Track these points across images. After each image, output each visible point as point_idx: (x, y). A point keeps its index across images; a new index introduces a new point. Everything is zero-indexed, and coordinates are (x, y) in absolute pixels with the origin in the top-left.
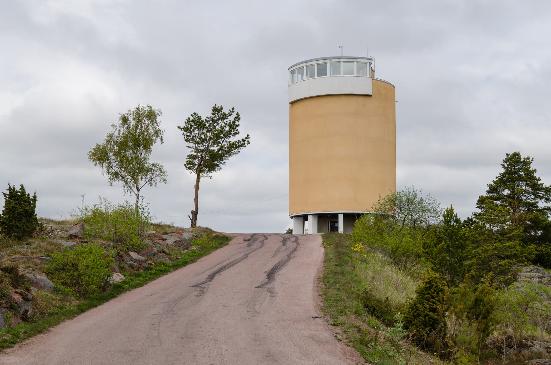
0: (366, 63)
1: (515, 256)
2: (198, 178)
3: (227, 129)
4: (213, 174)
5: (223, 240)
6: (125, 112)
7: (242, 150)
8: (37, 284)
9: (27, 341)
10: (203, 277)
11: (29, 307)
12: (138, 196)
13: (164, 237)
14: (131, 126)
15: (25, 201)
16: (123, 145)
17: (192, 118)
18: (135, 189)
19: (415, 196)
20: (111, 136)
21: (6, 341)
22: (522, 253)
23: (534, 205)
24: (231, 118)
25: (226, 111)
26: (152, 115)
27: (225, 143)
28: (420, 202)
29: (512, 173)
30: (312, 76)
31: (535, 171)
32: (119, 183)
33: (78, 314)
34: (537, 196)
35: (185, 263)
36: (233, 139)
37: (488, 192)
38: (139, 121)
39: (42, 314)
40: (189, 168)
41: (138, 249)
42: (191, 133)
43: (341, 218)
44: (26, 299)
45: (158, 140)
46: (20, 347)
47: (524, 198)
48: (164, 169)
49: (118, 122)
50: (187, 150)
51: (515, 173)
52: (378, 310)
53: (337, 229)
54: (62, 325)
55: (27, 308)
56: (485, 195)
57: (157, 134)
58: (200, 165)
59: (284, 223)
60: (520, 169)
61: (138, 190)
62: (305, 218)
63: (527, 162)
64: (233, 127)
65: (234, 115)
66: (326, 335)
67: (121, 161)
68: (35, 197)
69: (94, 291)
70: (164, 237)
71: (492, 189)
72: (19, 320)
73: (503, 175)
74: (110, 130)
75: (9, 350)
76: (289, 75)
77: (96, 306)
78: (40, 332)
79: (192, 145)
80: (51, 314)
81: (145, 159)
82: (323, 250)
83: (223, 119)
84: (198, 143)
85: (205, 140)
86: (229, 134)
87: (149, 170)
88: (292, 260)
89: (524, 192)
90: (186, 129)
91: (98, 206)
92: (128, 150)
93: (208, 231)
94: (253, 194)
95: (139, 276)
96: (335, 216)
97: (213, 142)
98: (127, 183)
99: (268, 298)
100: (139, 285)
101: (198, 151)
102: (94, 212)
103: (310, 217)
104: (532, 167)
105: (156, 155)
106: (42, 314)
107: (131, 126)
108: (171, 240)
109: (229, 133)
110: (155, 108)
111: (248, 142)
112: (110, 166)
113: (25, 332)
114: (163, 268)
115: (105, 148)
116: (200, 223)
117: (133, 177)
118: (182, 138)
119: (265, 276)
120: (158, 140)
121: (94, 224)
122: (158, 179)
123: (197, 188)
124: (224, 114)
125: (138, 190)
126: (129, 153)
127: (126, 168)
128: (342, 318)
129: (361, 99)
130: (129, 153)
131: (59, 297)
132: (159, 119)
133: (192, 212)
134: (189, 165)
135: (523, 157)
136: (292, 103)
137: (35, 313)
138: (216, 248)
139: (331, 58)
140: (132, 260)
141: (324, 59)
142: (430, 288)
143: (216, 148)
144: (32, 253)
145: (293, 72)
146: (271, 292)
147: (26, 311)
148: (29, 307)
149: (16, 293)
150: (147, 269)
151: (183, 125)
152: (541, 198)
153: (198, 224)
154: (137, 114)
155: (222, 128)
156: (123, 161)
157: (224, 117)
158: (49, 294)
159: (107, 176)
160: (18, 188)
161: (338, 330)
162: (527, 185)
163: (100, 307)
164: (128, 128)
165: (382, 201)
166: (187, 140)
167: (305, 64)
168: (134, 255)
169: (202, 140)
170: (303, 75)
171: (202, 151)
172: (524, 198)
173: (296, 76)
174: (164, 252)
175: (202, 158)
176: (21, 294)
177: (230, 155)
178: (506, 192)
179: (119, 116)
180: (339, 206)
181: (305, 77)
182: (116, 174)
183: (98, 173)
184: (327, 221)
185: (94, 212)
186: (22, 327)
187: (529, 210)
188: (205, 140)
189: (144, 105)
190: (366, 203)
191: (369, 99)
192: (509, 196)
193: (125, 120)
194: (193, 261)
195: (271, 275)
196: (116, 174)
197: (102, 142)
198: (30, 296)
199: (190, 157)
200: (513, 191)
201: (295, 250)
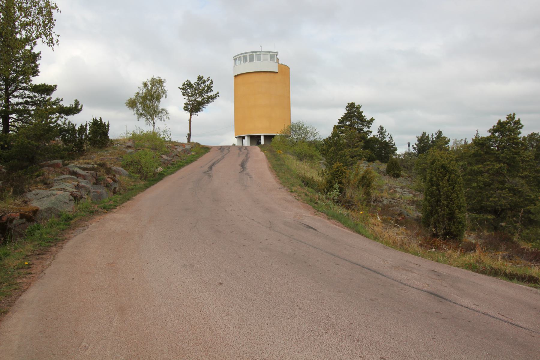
0: (274, 55)
1: (359, 155)
2: (191, 116)
3: (206, 88)
4: (199, 113)
5: (207, 149)
6: (145, 80)
7: (215, 100)
8: (119, 173)
9: (123, 205)
10: (206, 168)
11: (116, 185)
12: (154, 126)
13: (176, 147)
14: (149, 88)
15: (103, 127)
16: (144, 98)
17: (186, 83)
18: (152, 123)
19: (303, 125)
20: (138, 93)
21: (111, 205)
22: (363, 153)
23: (362, 130)
24: (208, 83)
25: (205, 78)
26: (160, 82)
27: (205, 96)
28: (306, 129)
29: (350, 113)
30: (246, 61)
31: (362, 112)
32: (143, 120)
33: (146, 189)
34: (363, 125)
35: (191, 162)
36: (209, 94)
37: (338, 123)
38: (153, 85)
39: (125, 189)
40: (186, 110)
41: (166, 153)
42: (186, 91)
43: (262, 138)
44: (115, 181)
45: (164, 95)
46: (120, 208)
47: (357, 126)
48: (168, 112)
49: (142, 86)
50: (183, 100)
51: (352, 113)
52: (307, 182)
53: (261, 143)
54: (139, 195)
55: (115, 186)
56: (337, 125)
57: (164, 92)
58: (191, 109)
59: (231, 140)
60: (355, 111)
61: (154, 123)
62: (243, 138)
63: (358, 107)
64: (209, 88)
65: (210, 81)
66: (290, 197)
67: (144, 107)
68: (108, 124)
69: (151, 176)
70: (176, 147)
71: (341, 122)
72: (112, 194)
73: (346, 114)
74: (137, 90)
75: (115, 210)
76: (233, 61)
77: (153, 185)
78: (128, 200)
79: (186, 97)
80: (130, 190)
81: (157, 106)
82: (263, 154)
83: (204, 83)
84: (190, 96)
85: (195, 94)
86: (207, 91)
87: (159, 112)
88: (249, 159)
89: (357, 123)
90: (183, 89)
91: (135, 131)
92: (148, 101)
93: (198, 144)
94: (218, 125)
95: (169, 168)
96: (259, 137)
97: (198, 96)
98: (148, 119)
99: (249, 178)
100: (172, 173)
101: (190, 101)
102: (133, 134)
103: (246, 138)
104: (361, 110)
105: (163, 104)
106: (125, 189)
107: (149, 88)
108: (180, 149)
109: (207, 91)
110: (162, 78)
111: (219, 96)
112: (138, 110)
113: (120, 200)
114: (181, 164)
115: (134, 100)
116: (193, 139)
117: (151, 116)
118: (181, 94)
119: (240, 167)
120: (164, 95)
121: (137, 141)
122: (165, 117)
123: (190, 121)
124: (205, 81)
125: (154, 123)
126: (148, 103)
127: (147, 111)
128: (294, 189)
129: (272, 74)
130: (148, 103)
131: (133, 180)
132: (164, 84)
133: (188, 134)
134: (186, 109)
135: (356, 105)
136: (236, 76)
137: (120, 189)
138: (205, 153)
139: (256, 52)
140: (164, 159)
141: (253, 52)
142: (338, 171)
143: (200, 99)
144: (111, 156)
145: (235, 60)
146: (210, 176)
147: (115, 188)
148: (116, 185)
149: (109, 178)
150: (172, 165)
151: (181, 87)
152: (365, 126)
153: (191, 141)
154: (152, 81)
155: (204, 88)
156: (145, 107)
157: (204, 82)
158: (127, 179)
159: (136, 116)
160: (98, 119)
161: (294, 194)
162: (358, 119)
163: (156, 185)
164: (147, 89)
165: (286, 128)
166: (184, 95)
167: (242, 55)
168: (165, 157)
169: (193, 95)
170: (241, 61)
171: (192, 101)
172: (357, 126)
173: (237, 61)
174: (177, 156)
175: (193, 105)
176: (111, 178)
177: (209, 103)
178: (348, 123)
179: (142, 83)
180: (262, 132)
181: (242, 62)
182: (141, 114)
183: (131, 114)
184: (255, 139)
185: (133, 134)
186: (108, 198)
187: (360, 132)
188: (195, 94)
189: (156, 77)
190: (276, 130)
191: (276, 74)
192: (349, 125)
193: (145, 85)
194: (195, 160)
195: (243, 165)
196: (141, 114)
197: (133, 97)
198: (117, 180)
199: (186, 104)
200: (351, 123)
201: (248, 153)
